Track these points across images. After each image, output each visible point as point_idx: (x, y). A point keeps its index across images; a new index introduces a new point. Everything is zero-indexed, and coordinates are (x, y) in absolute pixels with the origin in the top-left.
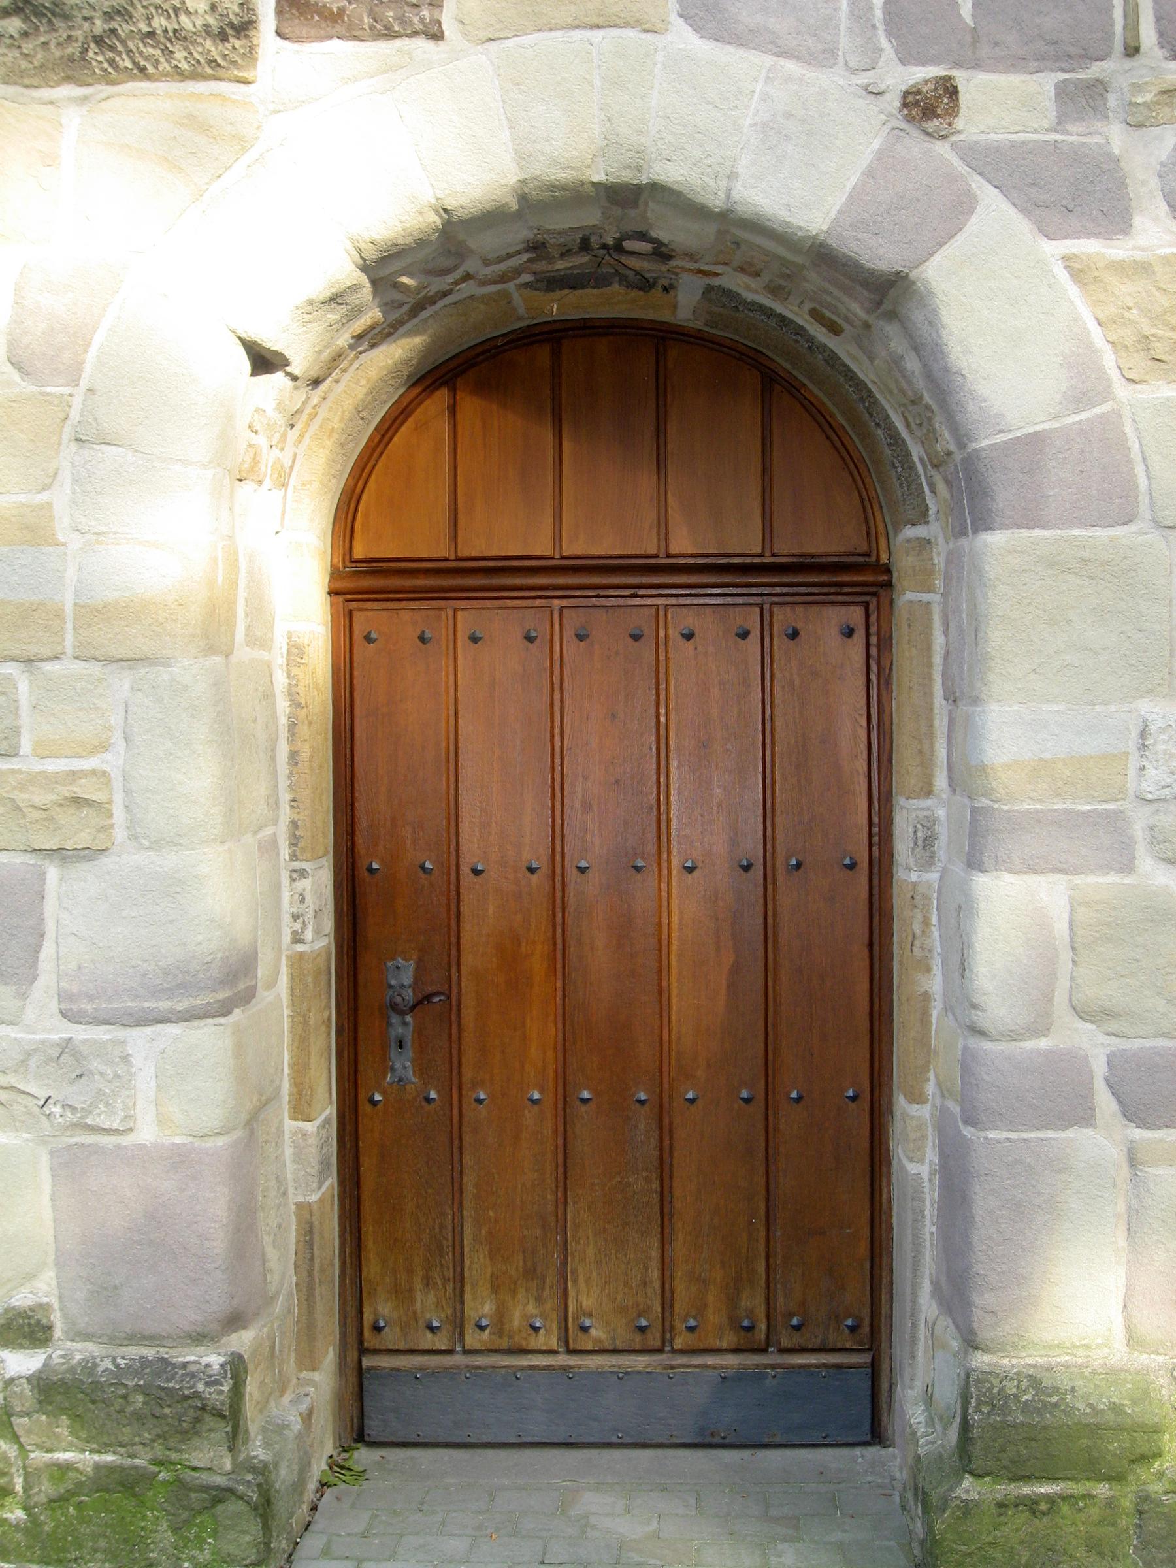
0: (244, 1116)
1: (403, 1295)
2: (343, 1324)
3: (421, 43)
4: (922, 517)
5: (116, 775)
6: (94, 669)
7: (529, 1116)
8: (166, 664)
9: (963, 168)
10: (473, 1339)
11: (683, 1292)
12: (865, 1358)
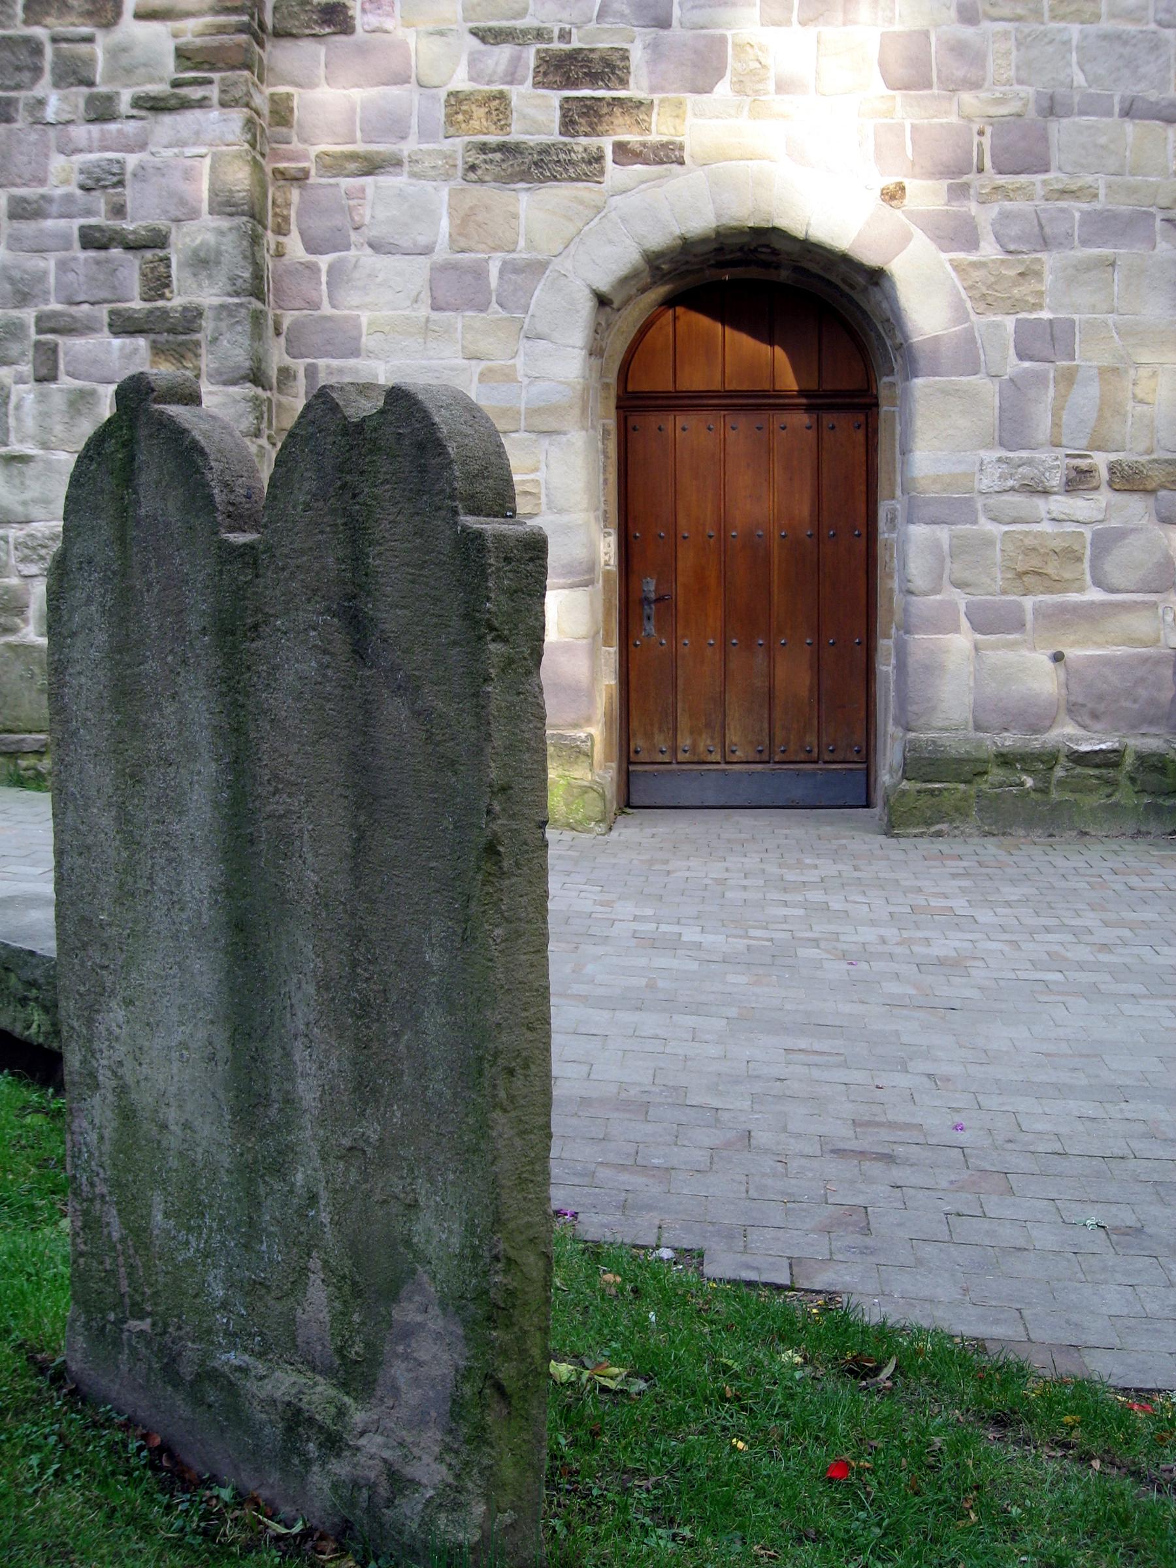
0: (592, 633)
1: (649, 736)
2: (621, 750)
3: (675, 166)
4: (891, 372)
5: (542, 481)
6: (533, 436)
7: (709, 651)
8: (565, 433)
9: (908, 222)
10: (681, 757)
11: (779, 734)
12: (863, 766)
